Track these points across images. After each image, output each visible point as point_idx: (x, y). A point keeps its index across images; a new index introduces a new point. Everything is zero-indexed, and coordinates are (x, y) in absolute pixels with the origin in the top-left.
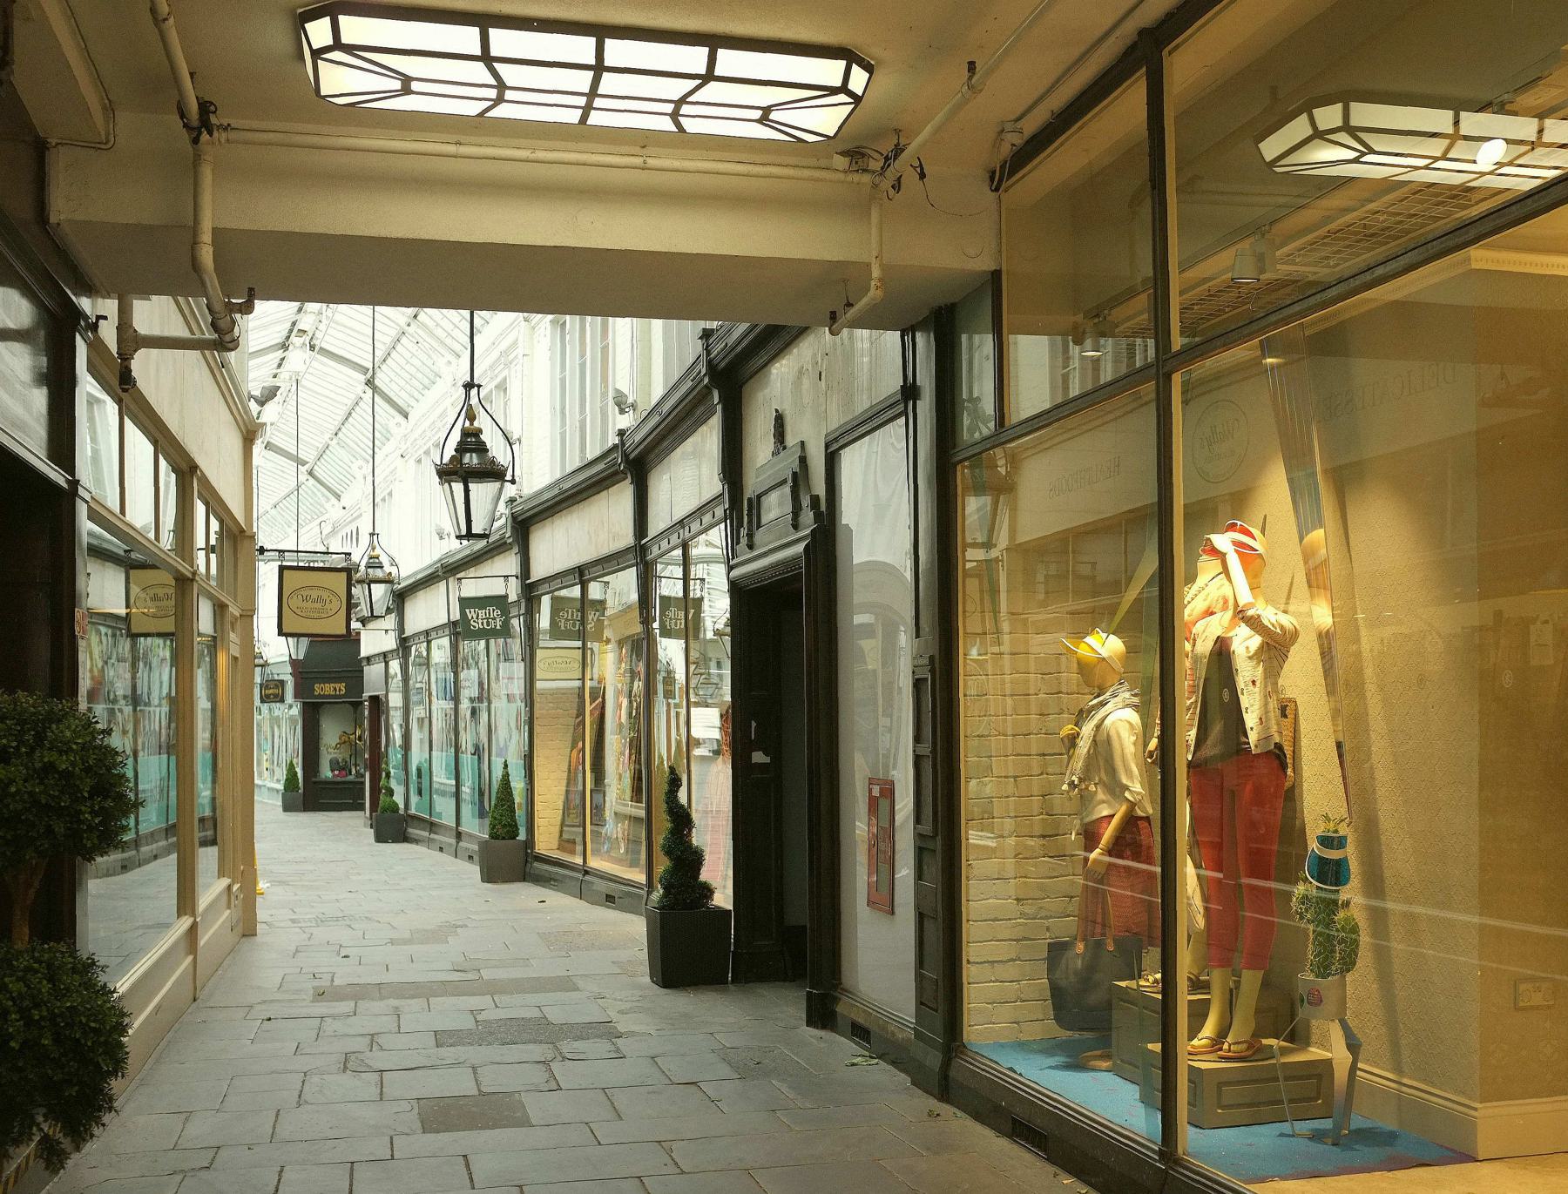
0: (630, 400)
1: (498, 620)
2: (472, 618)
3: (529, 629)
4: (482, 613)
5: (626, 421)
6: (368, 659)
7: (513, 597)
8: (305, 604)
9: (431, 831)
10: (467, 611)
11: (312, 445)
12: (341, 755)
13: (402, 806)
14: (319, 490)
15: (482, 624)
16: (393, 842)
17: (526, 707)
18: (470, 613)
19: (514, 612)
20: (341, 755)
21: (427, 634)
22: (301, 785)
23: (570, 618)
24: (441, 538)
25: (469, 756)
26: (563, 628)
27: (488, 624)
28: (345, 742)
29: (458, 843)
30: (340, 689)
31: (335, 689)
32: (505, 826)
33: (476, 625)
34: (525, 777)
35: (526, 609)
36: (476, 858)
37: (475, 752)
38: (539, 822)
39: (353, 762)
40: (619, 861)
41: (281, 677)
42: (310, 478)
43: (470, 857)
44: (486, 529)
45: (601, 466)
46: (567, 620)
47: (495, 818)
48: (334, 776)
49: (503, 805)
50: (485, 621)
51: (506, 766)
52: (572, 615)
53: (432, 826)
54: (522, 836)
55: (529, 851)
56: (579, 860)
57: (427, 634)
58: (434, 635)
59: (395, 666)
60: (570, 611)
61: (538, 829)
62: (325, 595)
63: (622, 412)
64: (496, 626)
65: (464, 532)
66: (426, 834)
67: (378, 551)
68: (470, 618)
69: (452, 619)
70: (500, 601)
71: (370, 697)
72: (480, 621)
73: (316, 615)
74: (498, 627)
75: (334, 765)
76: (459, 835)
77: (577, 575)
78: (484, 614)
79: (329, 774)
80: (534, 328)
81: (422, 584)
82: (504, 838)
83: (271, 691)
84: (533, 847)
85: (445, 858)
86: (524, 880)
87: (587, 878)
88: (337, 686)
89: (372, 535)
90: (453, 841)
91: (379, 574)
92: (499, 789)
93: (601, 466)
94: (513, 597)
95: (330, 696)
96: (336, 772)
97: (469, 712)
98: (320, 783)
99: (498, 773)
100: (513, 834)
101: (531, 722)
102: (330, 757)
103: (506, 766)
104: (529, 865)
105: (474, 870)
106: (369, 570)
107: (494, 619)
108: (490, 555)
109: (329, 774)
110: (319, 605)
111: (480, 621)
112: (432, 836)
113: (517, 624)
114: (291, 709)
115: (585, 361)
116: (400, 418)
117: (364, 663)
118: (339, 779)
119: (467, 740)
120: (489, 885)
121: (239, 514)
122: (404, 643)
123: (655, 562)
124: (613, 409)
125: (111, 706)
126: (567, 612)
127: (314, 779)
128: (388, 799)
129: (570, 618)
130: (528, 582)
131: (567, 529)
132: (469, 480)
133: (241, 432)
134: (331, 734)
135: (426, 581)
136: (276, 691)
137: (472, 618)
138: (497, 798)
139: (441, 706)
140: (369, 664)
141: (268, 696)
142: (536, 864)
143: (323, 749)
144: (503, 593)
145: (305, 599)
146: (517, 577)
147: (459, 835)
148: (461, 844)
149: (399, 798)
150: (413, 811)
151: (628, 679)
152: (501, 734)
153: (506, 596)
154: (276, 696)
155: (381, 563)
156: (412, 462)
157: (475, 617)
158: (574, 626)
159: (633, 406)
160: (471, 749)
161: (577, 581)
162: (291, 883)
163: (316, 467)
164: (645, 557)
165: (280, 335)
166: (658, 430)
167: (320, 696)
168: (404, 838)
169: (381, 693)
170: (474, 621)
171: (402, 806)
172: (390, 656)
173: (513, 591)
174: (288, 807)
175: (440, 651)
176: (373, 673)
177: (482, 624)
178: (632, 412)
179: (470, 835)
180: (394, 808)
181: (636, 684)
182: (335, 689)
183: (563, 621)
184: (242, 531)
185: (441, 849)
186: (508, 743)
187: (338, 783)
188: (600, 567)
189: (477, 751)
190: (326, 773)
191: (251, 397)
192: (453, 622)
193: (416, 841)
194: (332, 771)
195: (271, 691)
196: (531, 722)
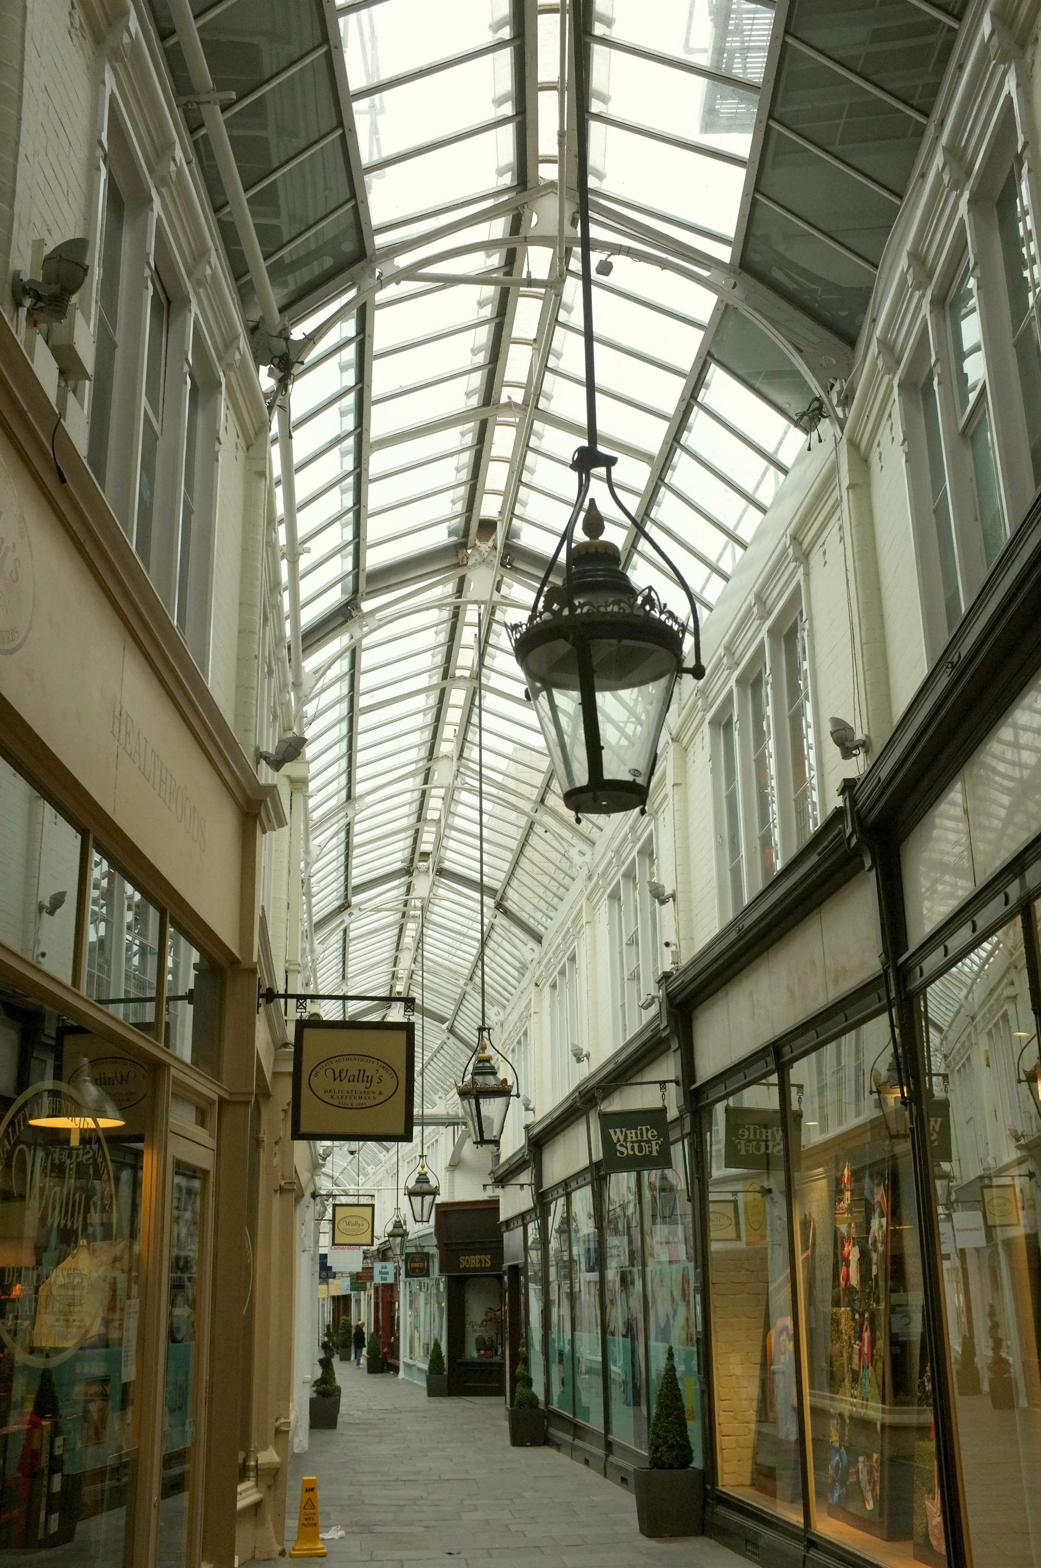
0: (859, 736)
1: (654, 1143)
2: (619, 1140)
3: (696, 1152)
4: (631, 1134)
5: (856, 767)
6: (507, 1223)
7: (673, 1113)
8: (337, 1085)
9: (575, 1436)
10: (611, 1131)
11: (448, 997)
12: (487, 1333)
13: (541, 1397)
14: (462, 1052)
15: (633, 1148)
16: (531, 1446)
17: (696, 1267)
18: (616, 1135)
19: (675, 1134)
20: (487, 1333)
21: (566, 1185)
22: (446, 1366)
23: (752, 1137)
24: (579, 1060)
25: (621, 1338)
26: (743, 1152)
27: (640, 1150)
28: (490, 1320)
29: (607, 1456)
30: (486, 1262)
31: (480, 1261)
32: (672, 1447)
33: (624, 1150)
34: (699, 1372)
35: (691, 1126)
36: (631, 1481)
37: (627, 1332)
38: (723, 1442)
39: (499, 1341)
40: (862, 1523)
41: (426, 1250)
42: (451, 1037)
43: (624, 1480)
44: (635, 772)
45: (814, 859)
46: (749, 1141)
47: (658, 1436)
48: (480, 1356)
49: (668, 1415)
50: (636, 1145)
51: (671, 1356)
52: (755, 1132)
53: (577, 1430)
54: (698, 1462)
55: (708, 1487)
56: (796, 1518)
57: (566, 1185)
58: (573, 1185)
59: (532, 1228)
60: (752, 1127)
61: (722, 1453)
62: (371, 1068)
63: (847, 753)
64: (651, 1152)
65: (582, 777)
66: (568, 1438)
67: (489, 1052)
68: (615, 1141)
69: (595, 1159)
70: (655, 1117)
71: (511, 1267)
72: (629, 1145)
73: (355, 1102)
74: (655, 1153)
75: (481, 1344)
76: (609, 1446)
77: (770, 1059)
78: (634, 1135)
79: (475, 1354)
80: (686, 749)
81: (561, 1123)
82: (671, 1467)
83: (416, 1265)
84: (714, 1482)
85: (591, 1476)
86: (703, 1533)
87: (813, 1554)
88: (483, 1257)
89: (481, 1030)
90: (601, 1452)
91: (491, 1081)
92: (661, 1390)
93: (814, 859)
94: (673, 1113)
95: (475, 1269)
96: (482, 1352)
97: (618, 1279)
98: (468, 1364)
99: (658, 1364)
100: (685, 1458)
101: (704, 1290)
102: (476, 1335)
103: (671, 1356)
104: (708, 1509)
105: (627, 1501)
106: (476, 1077)
107: (649, 1141)
108: (636, 1068)
109: (475, 1354)
110: (360, 1086)
111: (629, 1145)
112: (578, 1442)
113: (679, 1153)
114: (437, 1280)
115: (739, 864)
116: (532, 944)
117: (504, 1229)
118: (485, 1360)
119: (617, 1318)
120: (652, 1543)
121: (226, 931)
122: (542, 1202)
123: (922, 990)
124: (833, 751)
125: (179, 1275)
126: (749, 1130)
127: (459, 1361)
128: (525, 1391)
129: (752, 1137)
130: (693, 1087)
131: (751, 993)
132: (597, 682)
133: (237, 803)
134: (476, 1312)
135: (564, 1121)
136: (422, 1265)
137: (619, 1140)
138: (660, 1404)
139: (585, 1278)
140: (508, 1230)
141: (413, 1269)
142: (721, 1510)
143: (469, 1328)
144: (657, 1104)
145: (338, 1076)
146: (677, 1083)
147: (609, 1446)
148: (612, 1459)
149: (538, 1389)
150: (554, 1406)
151: (861, 1218)
152: (660, 1309)
153: (663, 1110)
154: (421, 1269)
155: (493, 1067)
156: (547, 990)
157: (622, 1138)
158: (758, 1149)
159: (865, 745)
160: (621, 1329)
161: (773, 1066)
162: (378, 1529)
163: (456, 1023)
164: (905, 987)
165: (399, 855)
166: (1003, 622)
167: (465, 1269)
168: (543, 1440)
169: (520, 1261)
170: (621, 1145)
171: (541, 1397)
172: (528, 1217)
173: (673, 1103)
174: (433, 1391)
175: (582, 1199)
176: (512, 1240)
177: (633, 1148)
178: (862, 755)
179: (624, 1448)
180: (533, 1401)
181: (875, 1223)
182: (480, 1261)
183: (743, 1142)
184: (234, 961)
185: (587, 1462)
186: (671, 1321)
187: (485, 1364)
188: (812, 1033)
189: (630, 1331)
190: (472, 1353)
191: (260, 756)
192: (596, 1164)
193: (558, 1446)
194: (478, 1350)
195: (416, 1265)
196: (704, 1290)
